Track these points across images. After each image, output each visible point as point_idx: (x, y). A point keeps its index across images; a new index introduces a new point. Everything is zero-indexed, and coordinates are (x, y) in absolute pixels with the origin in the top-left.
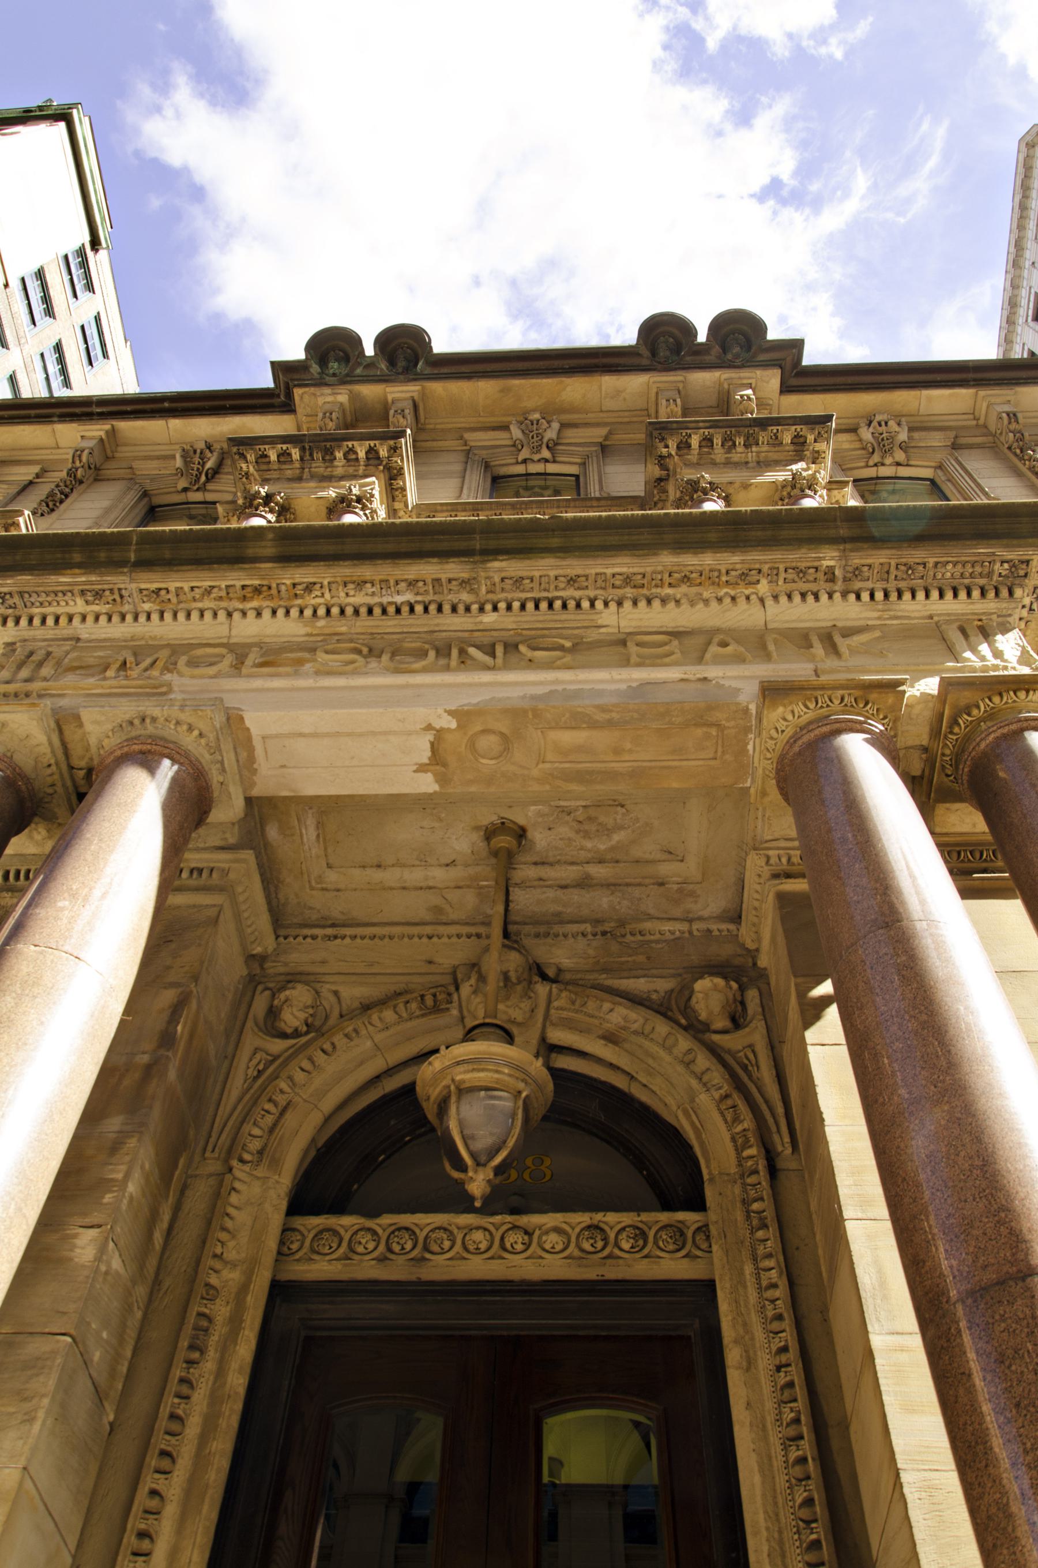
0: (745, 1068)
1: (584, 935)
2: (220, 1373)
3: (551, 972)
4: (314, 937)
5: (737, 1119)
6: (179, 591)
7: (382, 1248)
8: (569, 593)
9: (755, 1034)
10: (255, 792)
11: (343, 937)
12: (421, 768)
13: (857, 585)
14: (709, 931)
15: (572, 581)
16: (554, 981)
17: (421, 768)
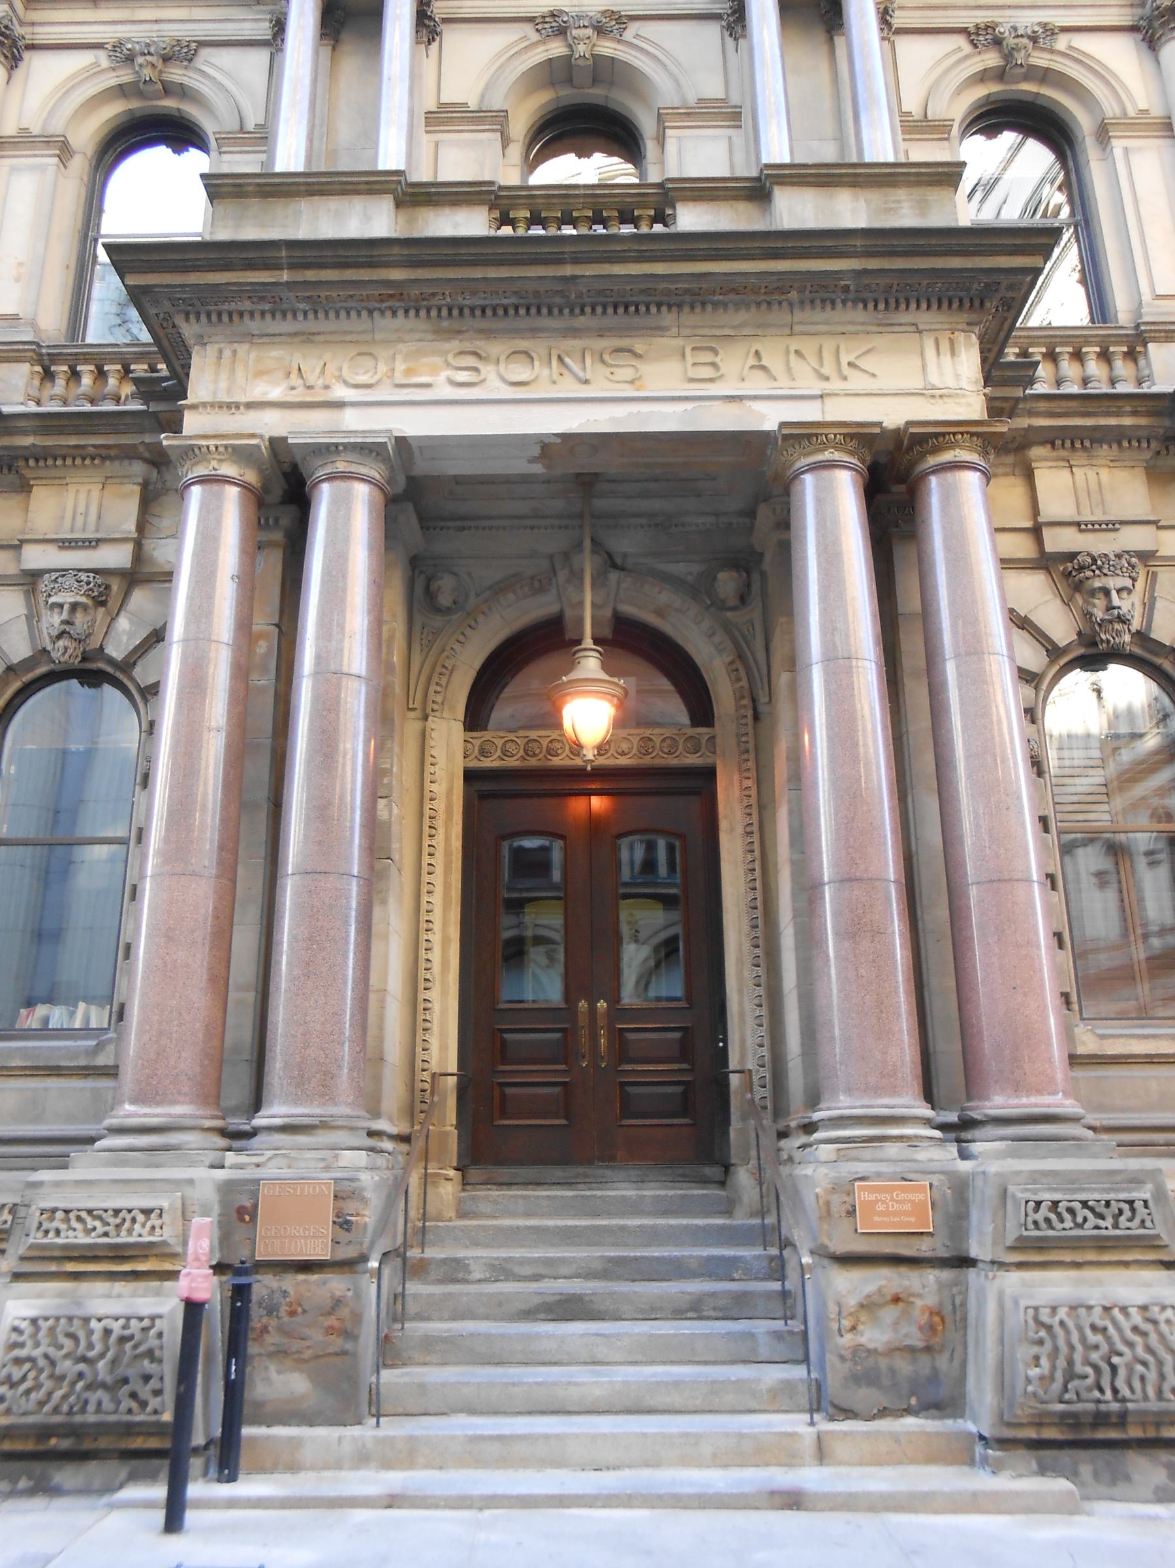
0: (745, 638)
1: (642, 526)
2: (447, 839)
3: (619, 561)
4: (449, 528)
5: (739, 680)
6: (327, 298)
7: (522, 753)
8: (642, 298)
9: (754, 612)
10: (413, 474)
11: (470, 528)
12: (532, 460)
13: (866, 295)
14: (731, 524)
15: (642, 291)
16: (623, 569)
17: (532, 460)
